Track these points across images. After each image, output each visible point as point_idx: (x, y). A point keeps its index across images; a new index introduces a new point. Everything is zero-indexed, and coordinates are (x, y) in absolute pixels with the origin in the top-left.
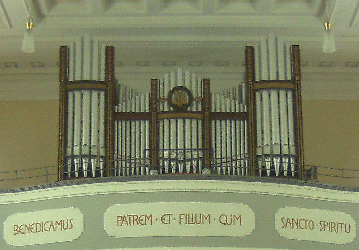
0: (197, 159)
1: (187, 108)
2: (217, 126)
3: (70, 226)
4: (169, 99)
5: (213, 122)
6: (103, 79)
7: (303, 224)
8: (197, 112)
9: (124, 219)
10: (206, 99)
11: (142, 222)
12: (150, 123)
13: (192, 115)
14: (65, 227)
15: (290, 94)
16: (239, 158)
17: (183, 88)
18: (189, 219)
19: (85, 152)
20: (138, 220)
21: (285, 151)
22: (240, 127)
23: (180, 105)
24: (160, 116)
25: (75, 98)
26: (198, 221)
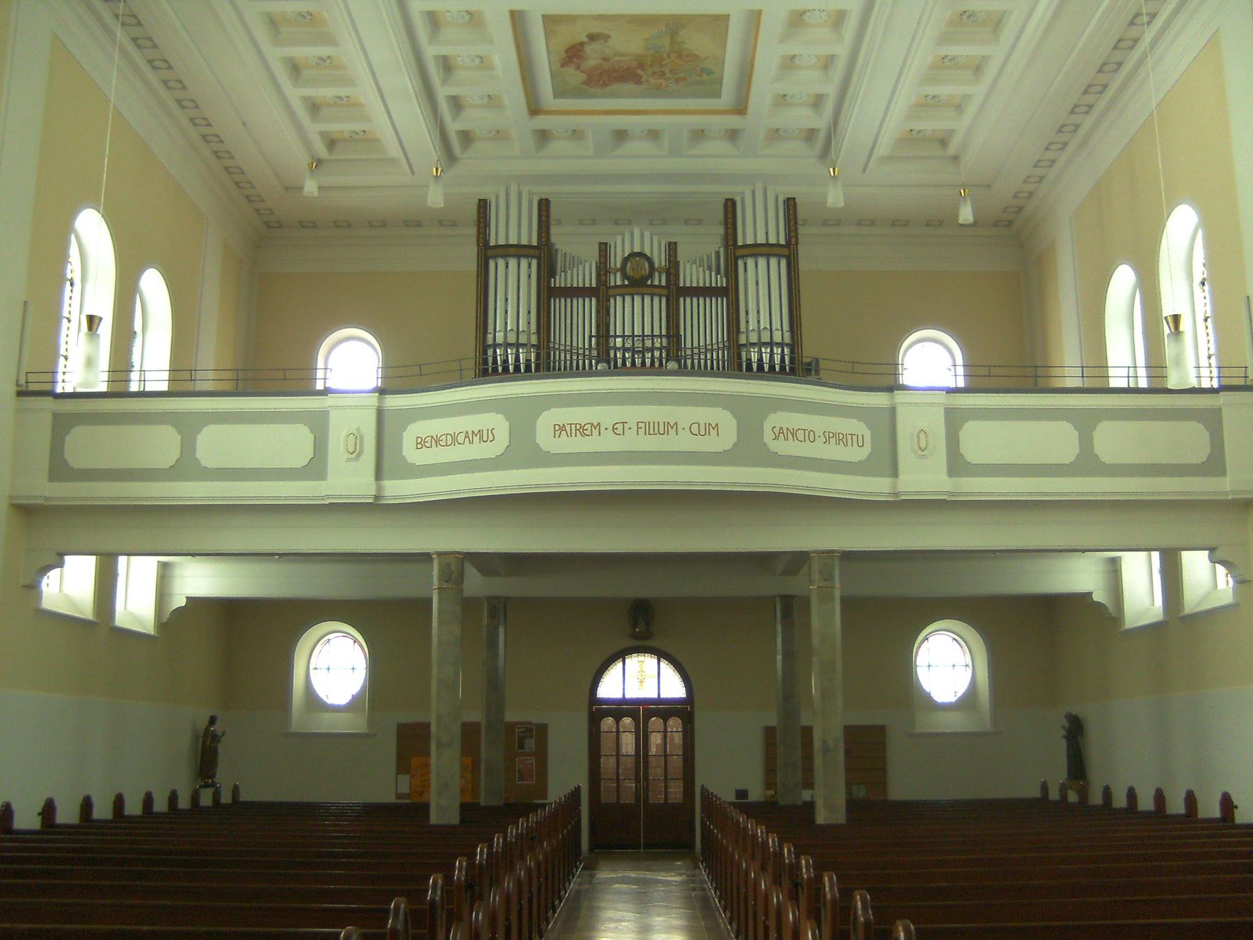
3: (491, 437)
7: (800, 435)
8: (660, 286)
9: (562, 428)
10: (673, 268)
12: (598, 301)
13: (653, 291)
15: (783, 263)
17: (641, 255)
18: (649, 428)
20: (581, 430)
22: (717, 307)
24: (611, 292)
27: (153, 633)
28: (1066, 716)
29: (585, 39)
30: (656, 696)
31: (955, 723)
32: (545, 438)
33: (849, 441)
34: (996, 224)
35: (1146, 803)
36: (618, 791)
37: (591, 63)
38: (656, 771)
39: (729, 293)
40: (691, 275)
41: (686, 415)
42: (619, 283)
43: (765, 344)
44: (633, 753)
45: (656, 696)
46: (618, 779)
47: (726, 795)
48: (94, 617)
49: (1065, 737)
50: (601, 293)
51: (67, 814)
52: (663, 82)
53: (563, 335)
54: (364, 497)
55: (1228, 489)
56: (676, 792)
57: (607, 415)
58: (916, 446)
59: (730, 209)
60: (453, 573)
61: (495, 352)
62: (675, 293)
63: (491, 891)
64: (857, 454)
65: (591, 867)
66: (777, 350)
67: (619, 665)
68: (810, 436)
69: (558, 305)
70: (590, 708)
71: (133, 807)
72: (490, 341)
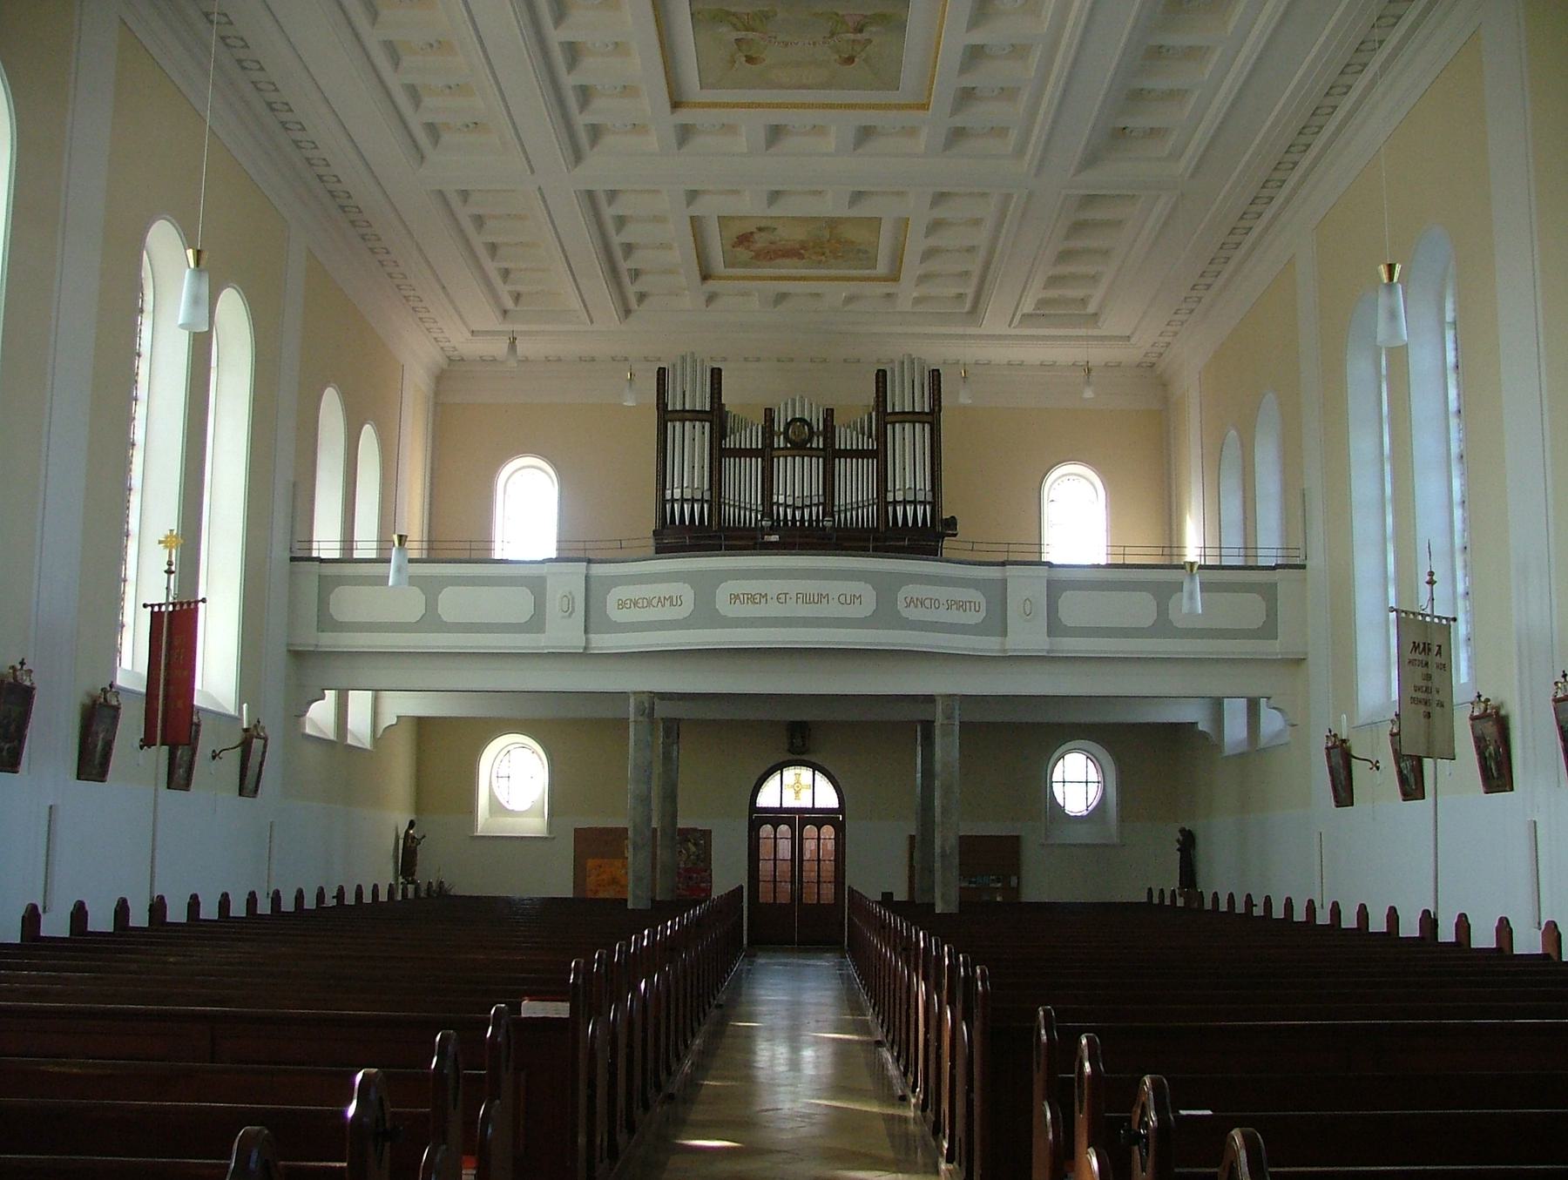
0: (817, 505)
1: (806, 444)
2: (841, 465)
3: (679, 603)
4: (786, 433)
5: (837, 460)
6: (708, 408)
7: (927, 603)
8: (818, 449)
9: (737, 597)
10: (829, 430)
11: (757, 601)
12: (763, 460)
13: (813, 452)
14: (674, 603)
15: (927, 427)
16: (866, 504)
17: (802, 420)
18: (805, 599)
19: (687, 495)
20: (752, 598)
21: (920, 497)
22: (869, 466)
23: (798, 440)
24: (775, 453)
25: (674, 428)
26: (816, 601)
27: (233, 713)
28: (1180, 831)
29: (755, 230)
30: (811, 806)
31: (1084, 836)
32: (723, 606)
33: (968, 608)
34: (1139, 365)
35: (1410, 927)
36: (775, 892)
37: (758, 245)
38: (810, 873)
39: (878, 454)
40: (844, 440)
41: (835, 588)
42: (782, 446)
43: (910, 502)
44: (789, 858)
45: (811, 806)
46: (775, 881)
47: (873, 894)
48: (235, 711)
49: (1178, 850)
50: (766, 454)
51: (101, 920)
52: (823, 258)
53: (727, 477)
54: (575, 648)
55: (1278, 651)
56: (828, 892)
57: (773, 587)
58: (1022, 611)
59: (881, 379)
60: (646, 708)
61: (673, 507)
62: (831, 454)
63: (1380, 387)
64: (973, 618)
65: (751, 956)
66: (920, 509)
67: (777, 776)
68: (935, 603)
69: (728, 463)
70: (750, 817)
71: (176, 913)
72: (668, 497)
